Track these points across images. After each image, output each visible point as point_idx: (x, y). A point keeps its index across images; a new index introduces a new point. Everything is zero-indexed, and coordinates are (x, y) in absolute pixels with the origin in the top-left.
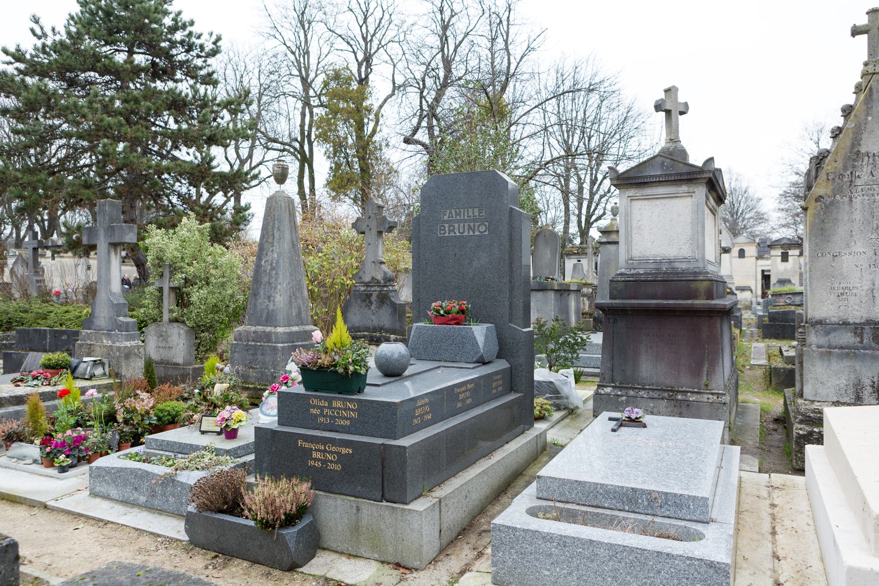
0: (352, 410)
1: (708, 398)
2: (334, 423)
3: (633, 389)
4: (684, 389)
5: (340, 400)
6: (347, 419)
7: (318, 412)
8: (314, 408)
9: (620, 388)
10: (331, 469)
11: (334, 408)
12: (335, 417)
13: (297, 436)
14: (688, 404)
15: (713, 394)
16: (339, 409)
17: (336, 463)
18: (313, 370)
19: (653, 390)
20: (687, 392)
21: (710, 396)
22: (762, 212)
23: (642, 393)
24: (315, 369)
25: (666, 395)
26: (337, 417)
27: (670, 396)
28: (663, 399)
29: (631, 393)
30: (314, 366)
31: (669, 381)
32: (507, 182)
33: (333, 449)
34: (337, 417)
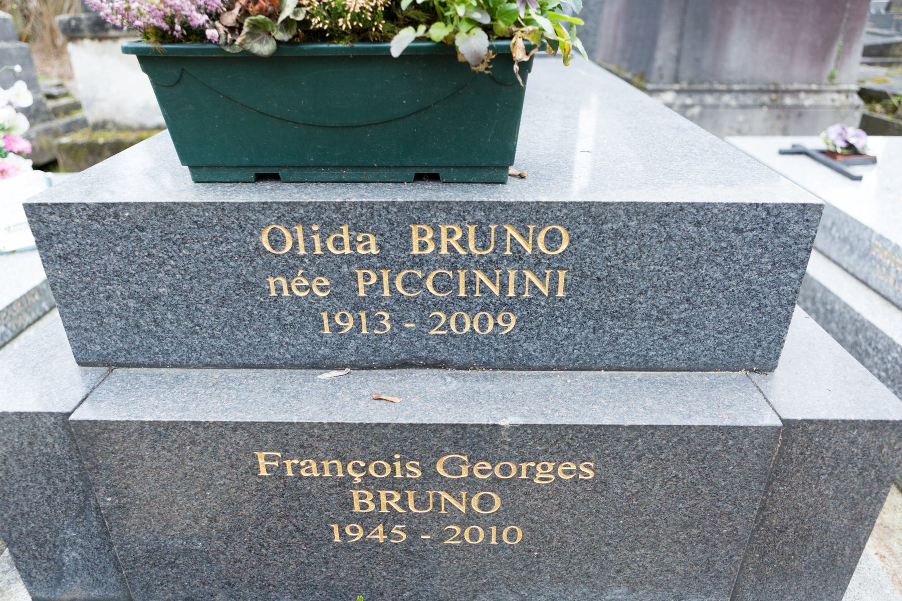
0: (538, 262)
1: (833, 100)
2: (420, 335)
3: (711, 91)
4: (796, 86)
5: (460, 219)
6: (501, 305)
7: (320, 287)
8: (288, 271)
9: (690, 92)
10: (465, 547)
11: (420, 262)
12: (426, 304)
13: (240, 437)
14: (799, 112)
15: (839, 92)
16: (454, 261)
17: (499, 521)
18: (248, 58)
19: (744, 92)
20: (798, 91)
21: (836, 96)
22: (201, 24)
23: (726, 98)
24: (264, 48)
25: (765, 98)
26: (438, 305)
27: (773, 101)
28: (761, 105)
29: (709, 99)
30: (257, 30)
31: (771, 74)
32: (8, 49)
33: (482, 470)
34: (438, 305)
